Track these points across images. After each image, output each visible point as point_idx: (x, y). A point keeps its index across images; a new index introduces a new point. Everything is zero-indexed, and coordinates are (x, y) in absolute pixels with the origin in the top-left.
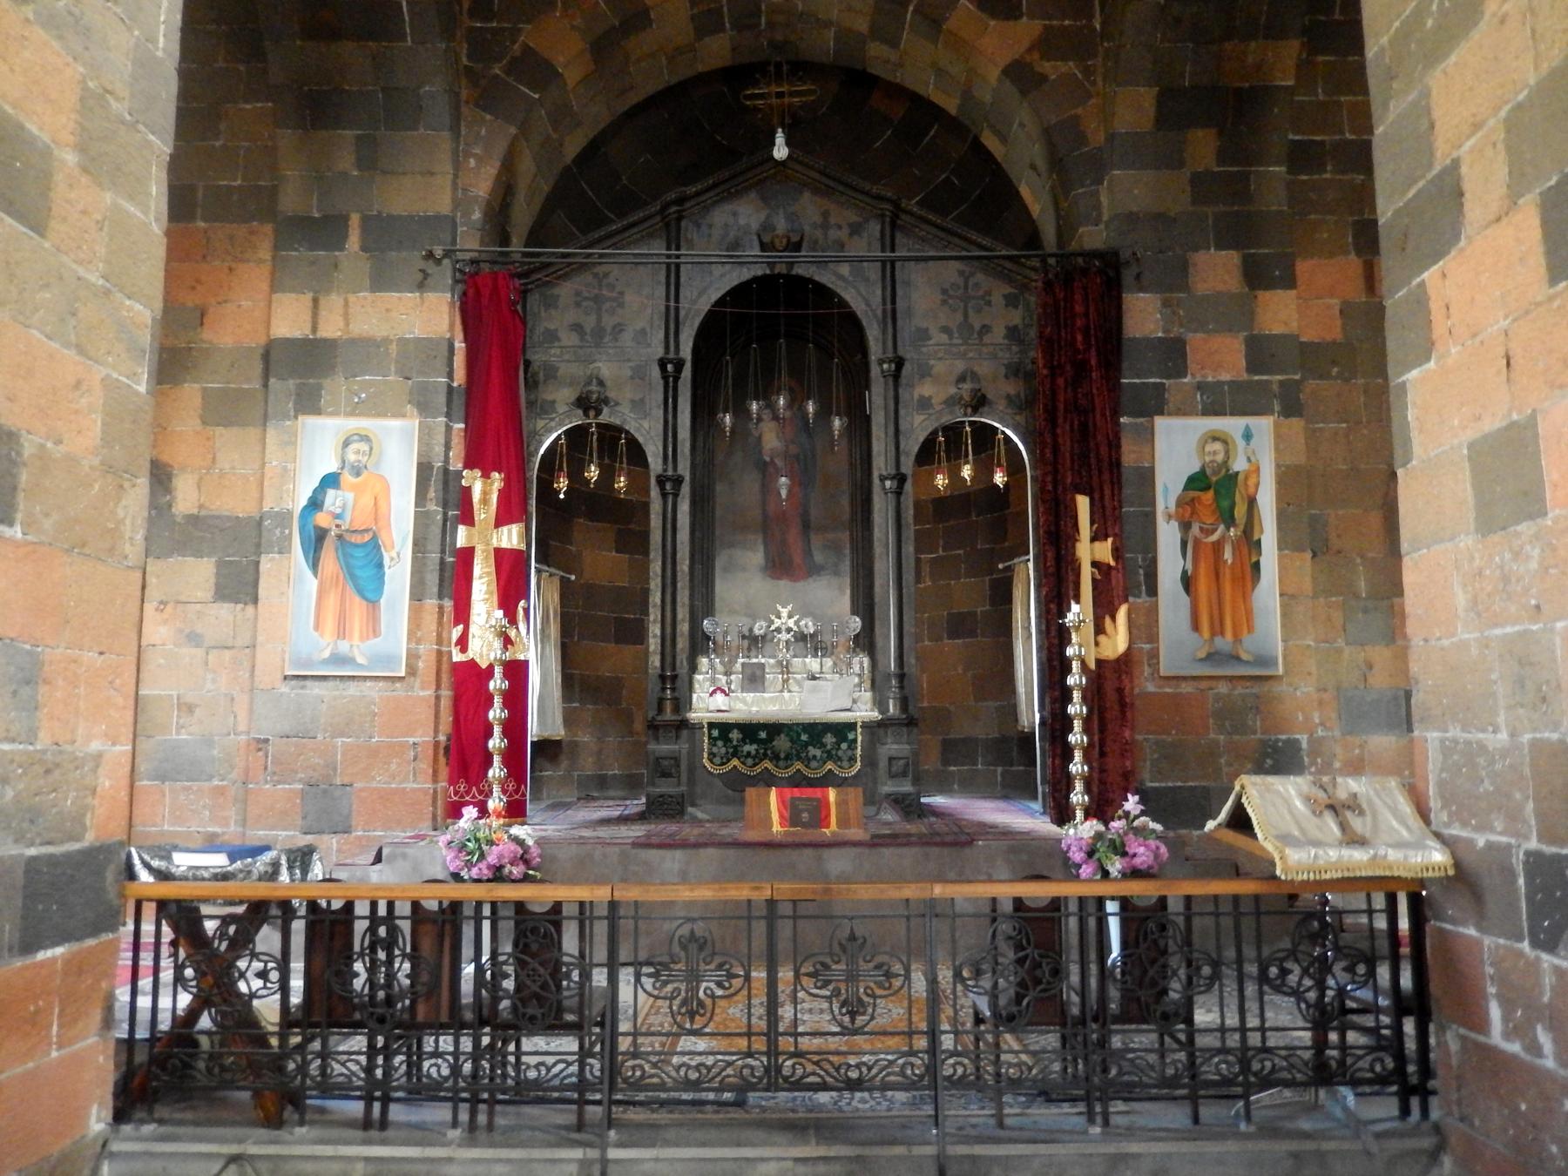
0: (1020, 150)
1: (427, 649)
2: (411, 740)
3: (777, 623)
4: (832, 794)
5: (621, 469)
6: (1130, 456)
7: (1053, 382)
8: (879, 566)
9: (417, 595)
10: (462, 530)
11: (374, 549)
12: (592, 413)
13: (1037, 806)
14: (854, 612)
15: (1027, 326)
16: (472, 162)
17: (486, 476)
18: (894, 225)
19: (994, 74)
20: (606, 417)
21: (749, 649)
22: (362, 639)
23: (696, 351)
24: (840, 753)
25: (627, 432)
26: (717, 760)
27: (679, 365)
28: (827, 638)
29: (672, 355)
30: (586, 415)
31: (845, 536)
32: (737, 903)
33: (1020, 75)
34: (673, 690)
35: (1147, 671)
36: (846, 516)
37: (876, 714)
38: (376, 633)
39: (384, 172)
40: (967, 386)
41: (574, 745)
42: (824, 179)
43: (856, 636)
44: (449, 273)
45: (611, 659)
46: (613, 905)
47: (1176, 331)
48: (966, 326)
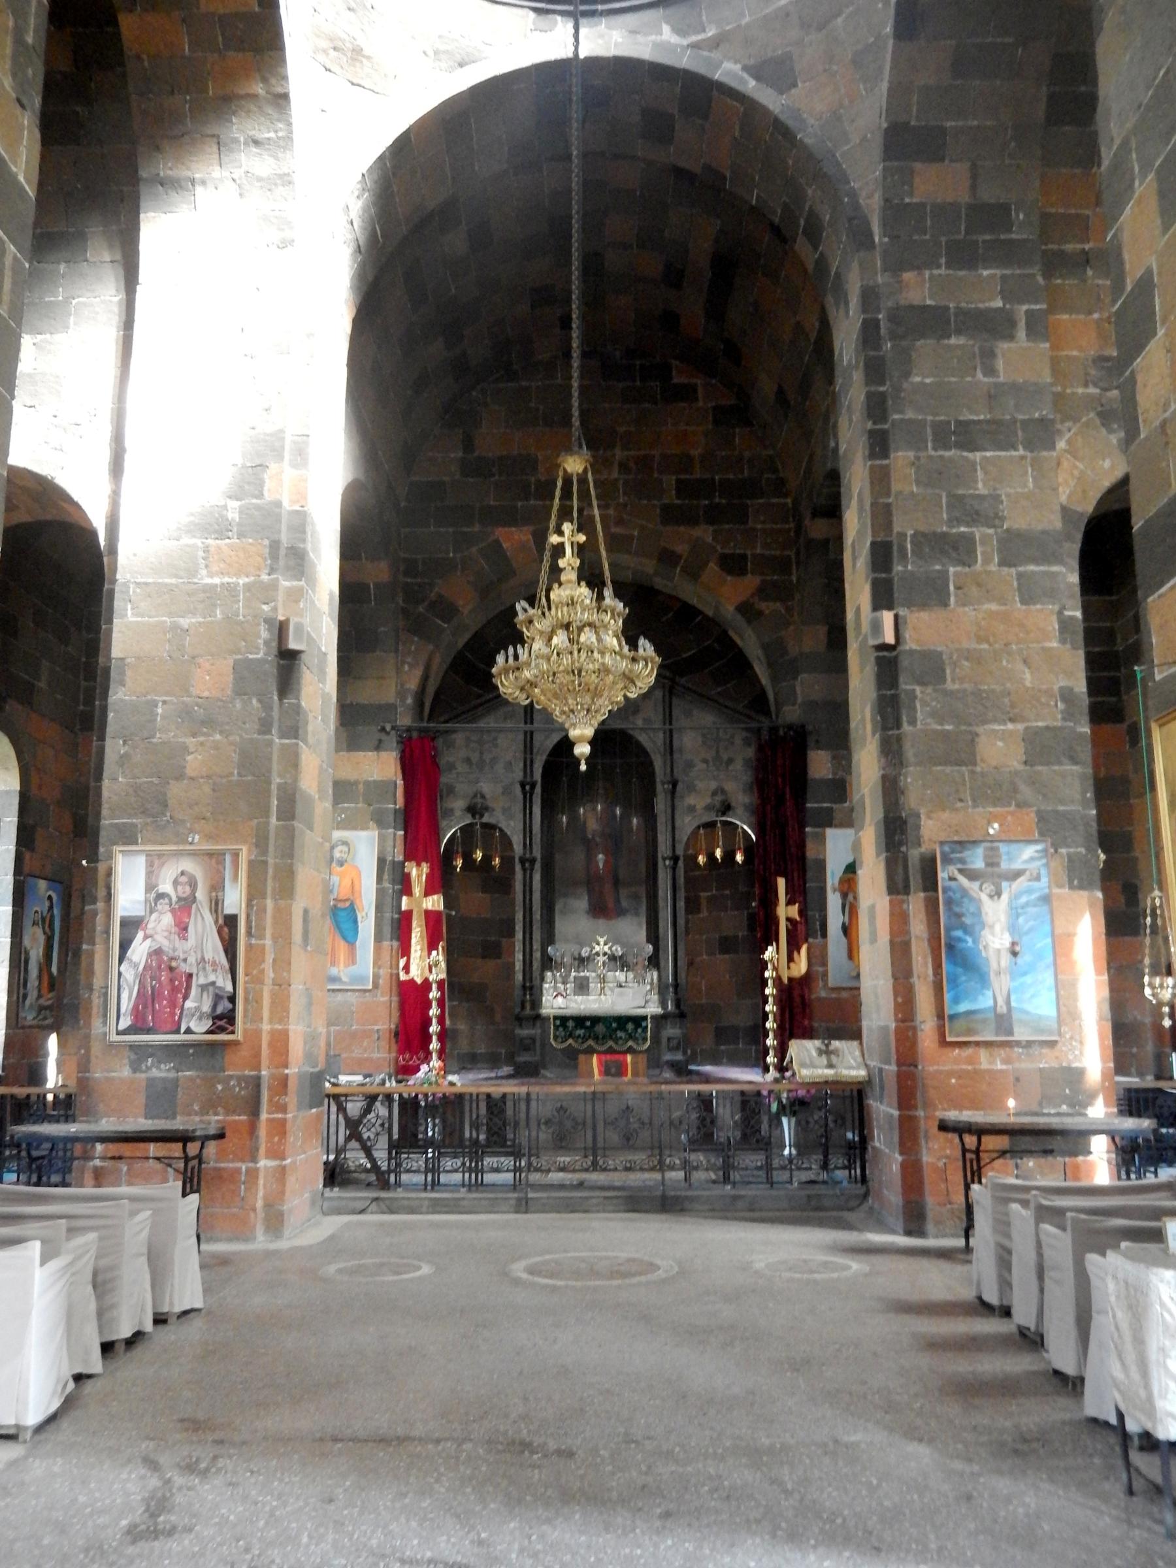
0: (750, 642)
1: (385, 972)
2: (376, 1028)
3: (597, 948)
6: (811, 853)
8: (661, 915)
9: (378, 938)
10: (404, 898)
11: (352, 912)
16: (406, 667)
17: (418, 865)
18: (671, 693)
19: (731, 608)
22: (346, 966)
23: (543, 776)
25: (501, 830)
26: (560, 1040)
28: (631, 959)
29: (528, 780)
30: (473, 816)
31: (642, 891)
32: (579, 1093)
33: (746, 610)
34: (531, 995)
35: (821, 984)
38: (354, 962)
39: (355, 678)
44: (394, 740)
45: (483, 970)
46: (528, 1094)
47: (840, 774)
48: (717, 757)
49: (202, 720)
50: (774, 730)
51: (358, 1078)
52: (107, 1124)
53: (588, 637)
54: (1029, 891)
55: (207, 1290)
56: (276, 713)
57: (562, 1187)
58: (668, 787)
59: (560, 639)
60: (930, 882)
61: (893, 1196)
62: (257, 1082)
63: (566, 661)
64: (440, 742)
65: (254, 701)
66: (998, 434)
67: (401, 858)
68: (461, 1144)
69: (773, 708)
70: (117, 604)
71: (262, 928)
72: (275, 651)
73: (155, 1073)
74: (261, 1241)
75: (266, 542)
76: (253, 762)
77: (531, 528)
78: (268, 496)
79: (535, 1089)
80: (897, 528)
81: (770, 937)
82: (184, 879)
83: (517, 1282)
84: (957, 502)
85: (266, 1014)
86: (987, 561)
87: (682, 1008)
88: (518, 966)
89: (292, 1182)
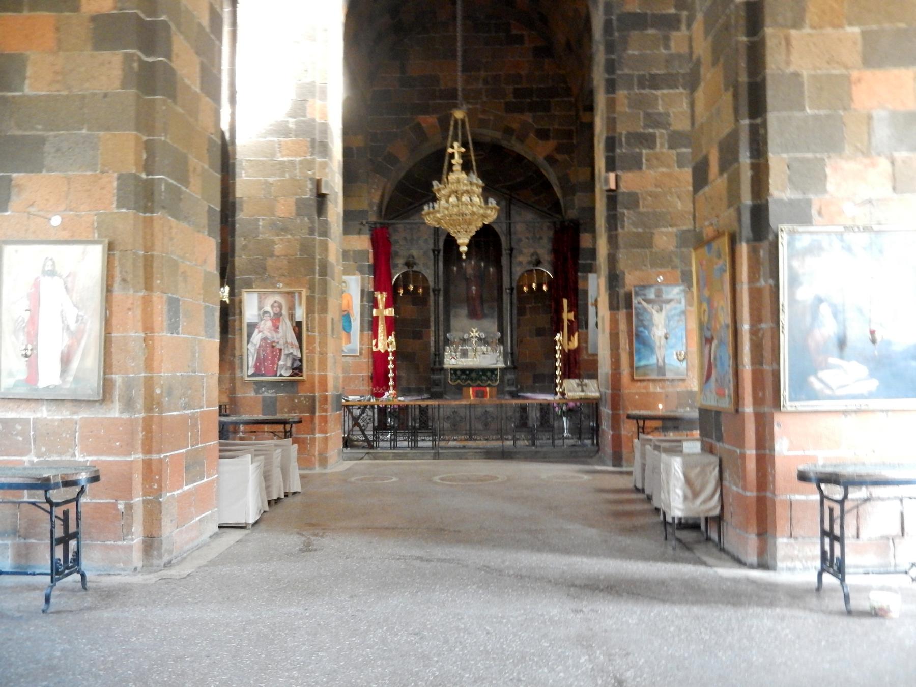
0: (552, 176)
4: (488, 389)
6: (581, 286)
9: (362, 330)
10: (374, 310)
20: (415, 268)
25: (423, 275)
27: (439, 251)
28: (490, 340)
31: (495, 304)
33: (550, 159)
45: (413, 345)
49: (282, 228)
50: (562, 223)
51: (358, 398)
52: (246, 417)
53: (465, 198)
54: (675, 309)
55: (302, 486)
56: (316, 225)
57: (455, 448)
58: (508, 252)
59: (453, 199)
60: (629, 305)
61: (608, 449)
62: (314, 397)
63: (455, 210)
64: (391, 229)
65: (306, 219)
66: (669, 81)
67: (372, 289)
68: (407, 428)
69: (563, 209)
70: (237, 170)
71: (313, 328)
72: (315, 194)
73: (266, 394)
74: (318, 470)
75: (309, 139)
76: (306, 248)
77: (438, 116)
78: (309, 116)
79: (441, 402)
80: (618, 130)
81: (559, 329)
82: (276, 305)
83: (435, 483)
84: (648, 116)
85: (316, 367)
86: (661, 147)
87: (516, 363)
88: (432, 344)
89: (330, 444)
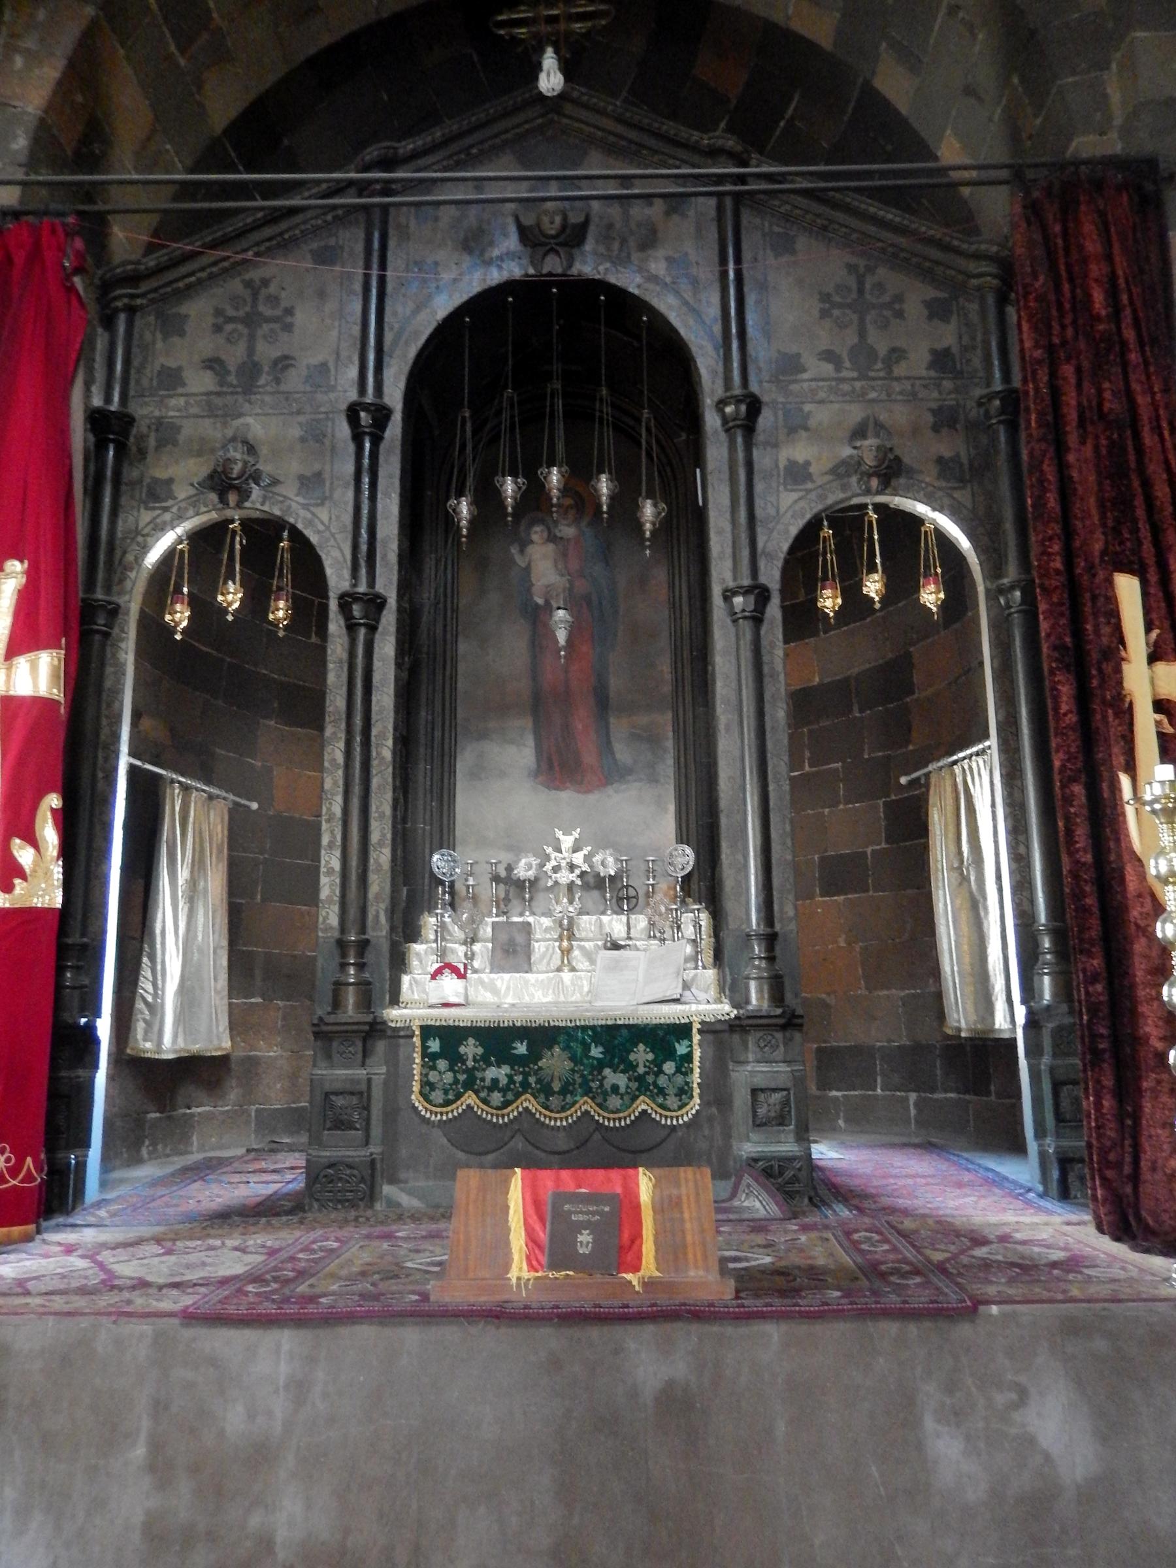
4: (645, 1184)
5: (280, 589)
7: (1053, 375)
12: (232, 498)
13: (1023, 1171)
14: (681, 839)
15: (965, 349)
20: (258, 503)
21: (507, 900)
24: (662, 1081)
25: (297, 536)
28: (639, 882)
29: (370, 398)
30: (223, 500)
34: (360, 966)
36: (667, 689)
37: (727, 1008)
40: (871, 442)
41: (252, 1064)
42: (620, 129)
43: (687, 879)
